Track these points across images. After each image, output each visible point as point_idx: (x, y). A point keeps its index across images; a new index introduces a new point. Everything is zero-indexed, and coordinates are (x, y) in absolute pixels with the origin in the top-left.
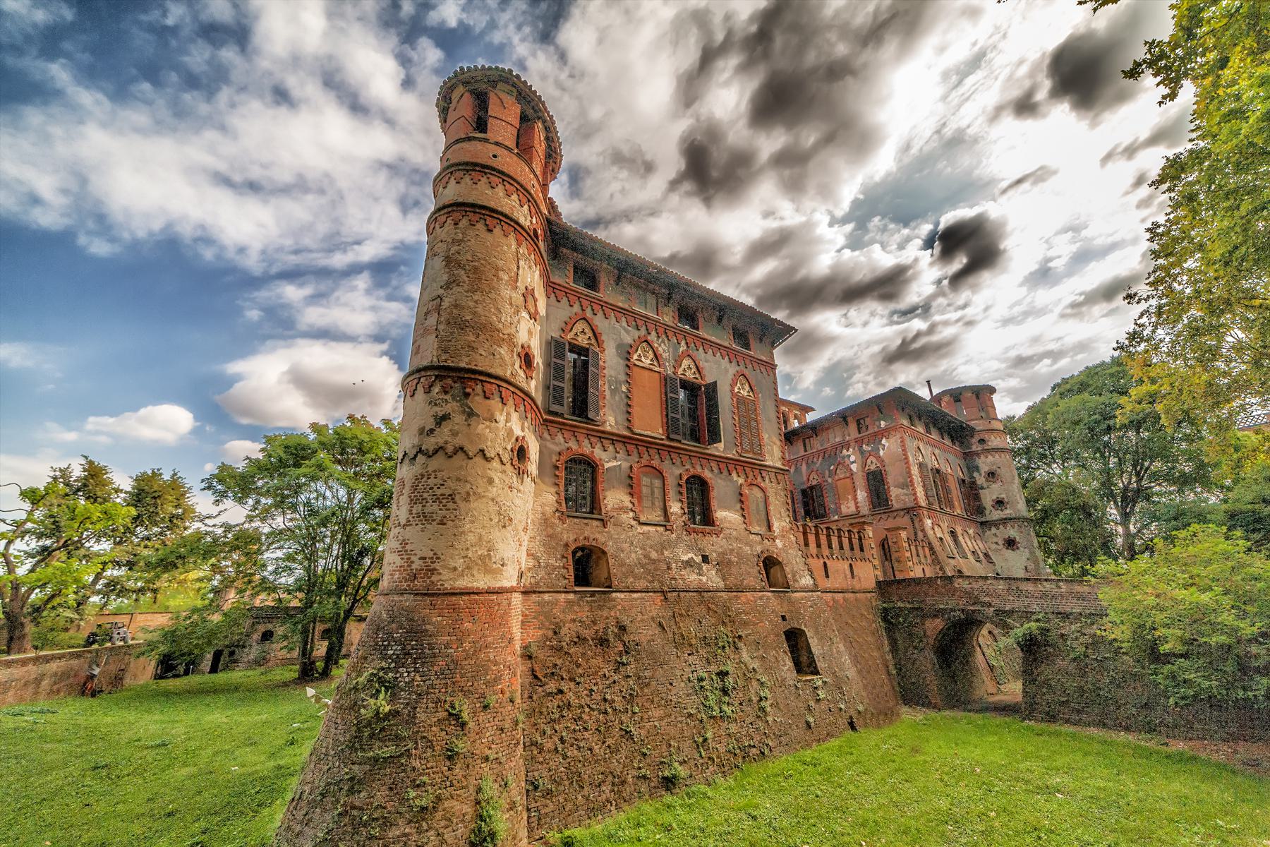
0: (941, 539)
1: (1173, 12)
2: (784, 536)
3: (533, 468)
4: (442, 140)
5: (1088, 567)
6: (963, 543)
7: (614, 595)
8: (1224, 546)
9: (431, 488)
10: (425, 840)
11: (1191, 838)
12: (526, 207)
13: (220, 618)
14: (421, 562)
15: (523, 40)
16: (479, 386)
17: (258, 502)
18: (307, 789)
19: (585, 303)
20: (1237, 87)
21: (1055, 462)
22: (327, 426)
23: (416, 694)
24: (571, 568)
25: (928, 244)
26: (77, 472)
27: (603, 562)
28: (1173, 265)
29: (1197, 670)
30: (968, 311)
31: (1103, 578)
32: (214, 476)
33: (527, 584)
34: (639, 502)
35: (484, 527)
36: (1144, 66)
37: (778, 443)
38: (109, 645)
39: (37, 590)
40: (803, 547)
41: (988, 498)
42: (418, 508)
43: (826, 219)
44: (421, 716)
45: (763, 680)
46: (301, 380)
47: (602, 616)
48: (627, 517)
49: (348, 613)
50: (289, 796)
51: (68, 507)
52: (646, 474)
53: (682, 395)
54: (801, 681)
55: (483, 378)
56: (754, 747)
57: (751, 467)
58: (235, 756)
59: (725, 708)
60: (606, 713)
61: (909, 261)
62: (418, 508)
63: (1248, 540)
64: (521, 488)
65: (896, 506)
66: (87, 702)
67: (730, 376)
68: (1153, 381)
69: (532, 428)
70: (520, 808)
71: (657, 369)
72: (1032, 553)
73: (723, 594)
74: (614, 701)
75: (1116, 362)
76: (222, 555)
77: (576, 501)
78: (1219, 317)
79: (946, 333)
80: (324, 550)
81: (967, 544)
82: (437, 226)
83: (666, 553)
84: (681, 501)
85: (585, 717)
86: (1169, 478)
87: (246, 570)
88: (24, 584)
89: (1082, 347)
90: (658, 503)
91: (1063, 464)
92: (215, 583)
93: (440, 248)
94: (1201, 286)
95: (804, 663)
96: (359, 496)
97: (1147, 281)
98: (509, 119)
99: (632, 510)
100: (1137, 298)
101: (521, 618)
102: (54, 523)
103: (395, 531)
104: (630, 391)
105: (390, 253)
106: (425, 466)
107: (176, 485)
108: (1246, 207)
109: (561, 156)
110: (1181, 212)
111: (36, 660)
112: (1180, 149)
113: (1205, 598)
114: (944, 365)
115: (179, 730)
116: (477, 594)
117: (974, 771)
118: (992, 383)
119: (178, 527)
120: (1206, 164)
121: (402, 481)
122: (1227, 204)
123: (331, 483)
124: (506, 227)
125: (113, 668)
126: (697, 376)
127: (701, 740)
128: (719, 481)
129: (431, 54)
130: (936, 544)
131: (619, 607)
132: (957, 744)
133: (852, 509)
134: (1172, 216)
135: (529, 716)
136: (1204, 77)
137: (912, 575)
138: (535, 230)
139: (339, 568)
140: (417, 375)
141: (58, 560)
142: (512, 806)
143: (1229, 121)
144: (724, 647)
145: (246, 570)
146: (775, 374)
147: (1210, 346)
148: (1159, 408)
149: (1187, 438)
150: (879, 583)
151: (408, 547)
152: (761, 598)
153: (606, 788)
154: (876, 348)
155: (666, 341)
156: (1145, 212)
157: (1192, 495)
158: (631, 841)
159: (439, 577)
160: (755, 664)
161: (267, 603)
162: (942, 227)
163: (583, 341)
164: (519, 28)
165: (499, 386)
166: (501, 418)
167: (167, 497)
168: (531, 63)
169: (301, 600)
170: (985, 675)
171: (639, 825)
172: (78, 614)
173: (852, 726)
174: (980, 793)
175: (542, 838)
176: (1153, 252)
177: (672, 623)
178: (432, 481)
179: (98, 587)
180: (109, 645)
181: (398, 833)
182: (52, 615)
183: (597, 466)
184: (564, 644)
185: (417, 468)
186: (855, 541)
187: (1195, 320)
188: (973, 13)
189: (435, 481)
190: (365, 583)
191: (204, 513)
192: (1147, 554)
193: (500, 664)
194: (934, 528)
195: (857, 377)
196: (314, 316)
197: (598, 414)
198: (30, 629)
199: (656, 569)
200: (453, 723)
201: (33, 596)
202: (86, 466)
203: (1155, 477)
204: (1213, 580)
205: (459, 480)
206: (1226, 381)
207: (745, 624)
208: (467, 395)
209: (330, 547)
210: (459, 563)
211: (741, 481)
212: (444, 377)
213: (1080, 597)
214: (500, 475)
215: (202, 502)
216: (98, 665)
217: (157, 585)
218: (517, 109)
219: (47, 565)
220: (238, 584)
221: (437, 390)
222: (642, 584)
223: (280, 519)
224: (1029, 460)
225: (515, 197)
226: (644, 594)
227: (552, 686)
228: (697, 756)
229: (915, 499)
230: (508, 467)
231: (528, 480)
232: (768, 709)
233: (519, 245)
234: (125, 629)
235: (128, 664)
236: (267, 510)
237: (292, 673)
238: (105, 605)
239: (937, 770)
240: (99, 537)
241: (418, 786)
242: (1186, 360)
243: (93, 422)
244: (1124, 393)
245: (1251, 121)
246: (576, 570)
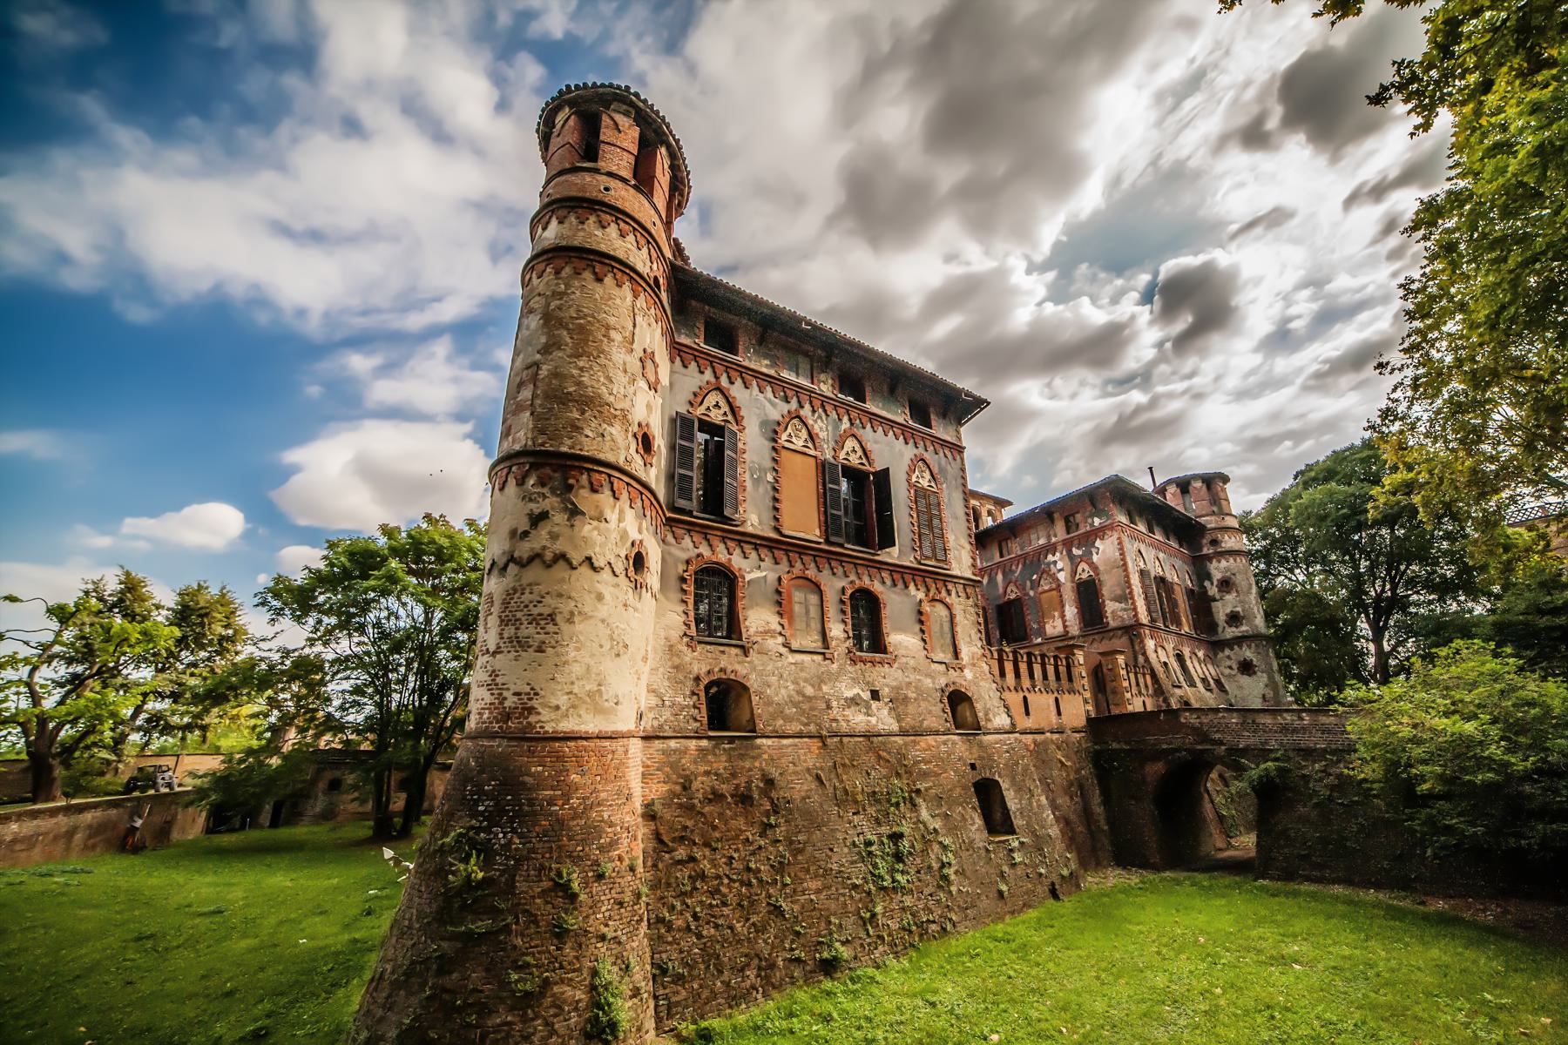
0: (1165, 664)
1: (1428, 26)
2: (974, 665)
3: (653, 578)
4: (542, 172)
5: (1335, 693)
6: (1192, 671)
7: (759, 741)
8: (1492, 665)
9: (527, 606)
10: (531, 1030)
11: (1454, 1016)
12: (645, 250)
13: (279, 762)
14: (515, 699)
15: (644, 51)
16: (585, 477)
17: (320, 622)
18: (389, 967)
19: (720, 369)
20: (1503, 115)
21: (1298, 567)
22: (398, 528)
23: (514, 859)
24: (704, 708)
25: (1147, 298)
26: (112, 585)
27: (745, 700)
28: (1430, 328)
29: (1460, 815)
30: (1196, 381)
31: (1351, 706)
32: (269, 590)
33: (649, 728)
34: (790, 623)
35: (592, 655)
36: (1392, 91)
37: (968, 547)
38: (152, 792)
39: (68, 726)
40: (998, 678)
41: (1221, 611)
42: (509, 631)
43: (1023, 265)
44: (521, 886)
45: (946, 842)
46: (368, 471)
47: (743, 767)
48: (775, 644)
49: (430, 759)
50: (367, 975)
51: (102, 626)
52: (798, 587)
53: (844, 485)
54: (993, 842)
55: (590, 466)
56: (934, 922)
57: (933, 577)
58: (301, 927)
59: (899, 877)
60: (749, 884)
61: (1126, 317)
62: (509, 631)
63: (1521, 658)
64: (639, 606)
65: (1112, 624)
66: (126, 861)
67: (906, 461)
68: (1410, 468)
69: (652, 529)
70: (645, 995)
71: (812, 452)
72: (1271, 678)
73: (897, 738)
74: (759, 870)
75: (1367, 444)
76: (280, 686)
77: (709, 623)
78: (1484, 391)
79: (1172, 407)
80: (398, 682)
81: (1197, 669)
82: (534, 275)
83: (825, 688)
84: (844, 622)
85: (724, 890)
86: (1430, 586)
87: (308, 704)
88: (52, 718)
89: (1330, 425)
90: (815, 625)
91: (1307, 569)
92: (273, 719)
93: (537, 303)
94: (1463, 353)
95: (997, 820)
96: (438, 615)
97: (1401, 348)
98: (625, 145)
99: (780, 634)
100: (1389, 368)
101: (641, 769)
102: (86, 646)
103: (482, 660)
104: (777, 481)
105: (476, 311)
106: (518, 577)
107: (223, 600)
108: (1515, 258)
109: (690, 187)
110: (1438, 265)
111: (67, 810)
112: (1433, 192)
113: (1470, 727)
114: (1169, 448)
115: (237, 894)
116: (586, 739)
117: (1197, 941)
118: (1225, 471)
119: (228, 651)
120: (1467, 207)
121: (490, 596)
122: (1493, 255)
123: (404, 598)
124: (619, 275)
125: (157, 819)
126: (864, 461)
127: (868, 915)
128: (893, 596)
129: (531, 72)
130: (1160, 670)
131: (766, 756)
132: (1178, 911)
133: (1059, 629)
134: (1427, 270)
135: (653, 888)
136: (1463, 103)
137: (1130, 708)
138: (656, 278)
139: (417, 704)
140: (507, 464)
141: (91, 690)
142: (636, 993)
143: (1494, 156)
144: (897, 804)
145: (308, 704)
146: (962, 459)
147: (1474, 426)
148: (1416, 499)
149: (1449, 536)
150: (1089, 720)
151: (499, 680)
152: (945, 743)
153: (751, 973)
154: (1087, 426)
155: (824, 417)
156: (1397, 265)
157: (1455, 604)
158: (782, 1033)
159: (538, 718)
160: (937, 824)
161: (333, 745)
162: (1161, 277)
163: (716, 417)
164: (640, 37)
165: (610, 476)
166: (612, 516)
167: (215, 614)
168: (652, 78)
169: (372, 743)
170: (1214, 829)
171: (791, 1015)
172: (116, 755)
173: (1054, 894)
174: (1203, 966)
175: (672, 1030)
176: (1408, 313)
177: (833, 776)
178: (527, 597)
179: (139, 722)
180: (152, 792)
181: (498, 1021)
182: (86, 755)
183: (736, 577)
184: (696, 801)
185: (508, 581)
186: (1062, 669)
187: (1457, 394)
188: (1189, 25)
189: (531, 597)
190: (448, 723)
191: (258, 636)
192: (1402, 677)
193: (616, 825)
194: (1159, 651)
195: (1065, 462)
196: (385, 391)
197: (736, 511)
198: (59, 772)
199: (812, 709)
200: (560, 894)
201: (63, 733)
202: (123, 578)
203: (1412, 583)
204: (1479, 706)
205: (560, 595)
206: (1493, 467)
207: (925, 775)
208: (570, 488)
209: (405, 677)
210: (563, 701)
211: (921, 595)
212: (542, 465)
213: (1326, 730)
214: (612, 589)
215: (254, 621)
216: (140, 817)
217: (207, 720)
218: (635, 132)
219: (78, 696)
220: (299, 722)
221: (532, 482)
222: (794, 727)
223: (345, 643)
224: (1268, 564)
225: (631, 238)
226: (797, 740)
227: (681, 853)
228: (863, 934)
229: (1136, 615)
230: (622, 579)
231: (647, 596)
232: (953, 877)
233: (636, 296)
234: (170, 773)
235: (174, 817)
236: (329, 632)
237: (364, 830)
238: (147, 744)
239: (1154, 941)
240: (139, 661)
241: (521, 967)
242: (1446, 442)
243: (131, 525)
244: (1377, 481)
245: (1520, 156)
246: (709, 709)
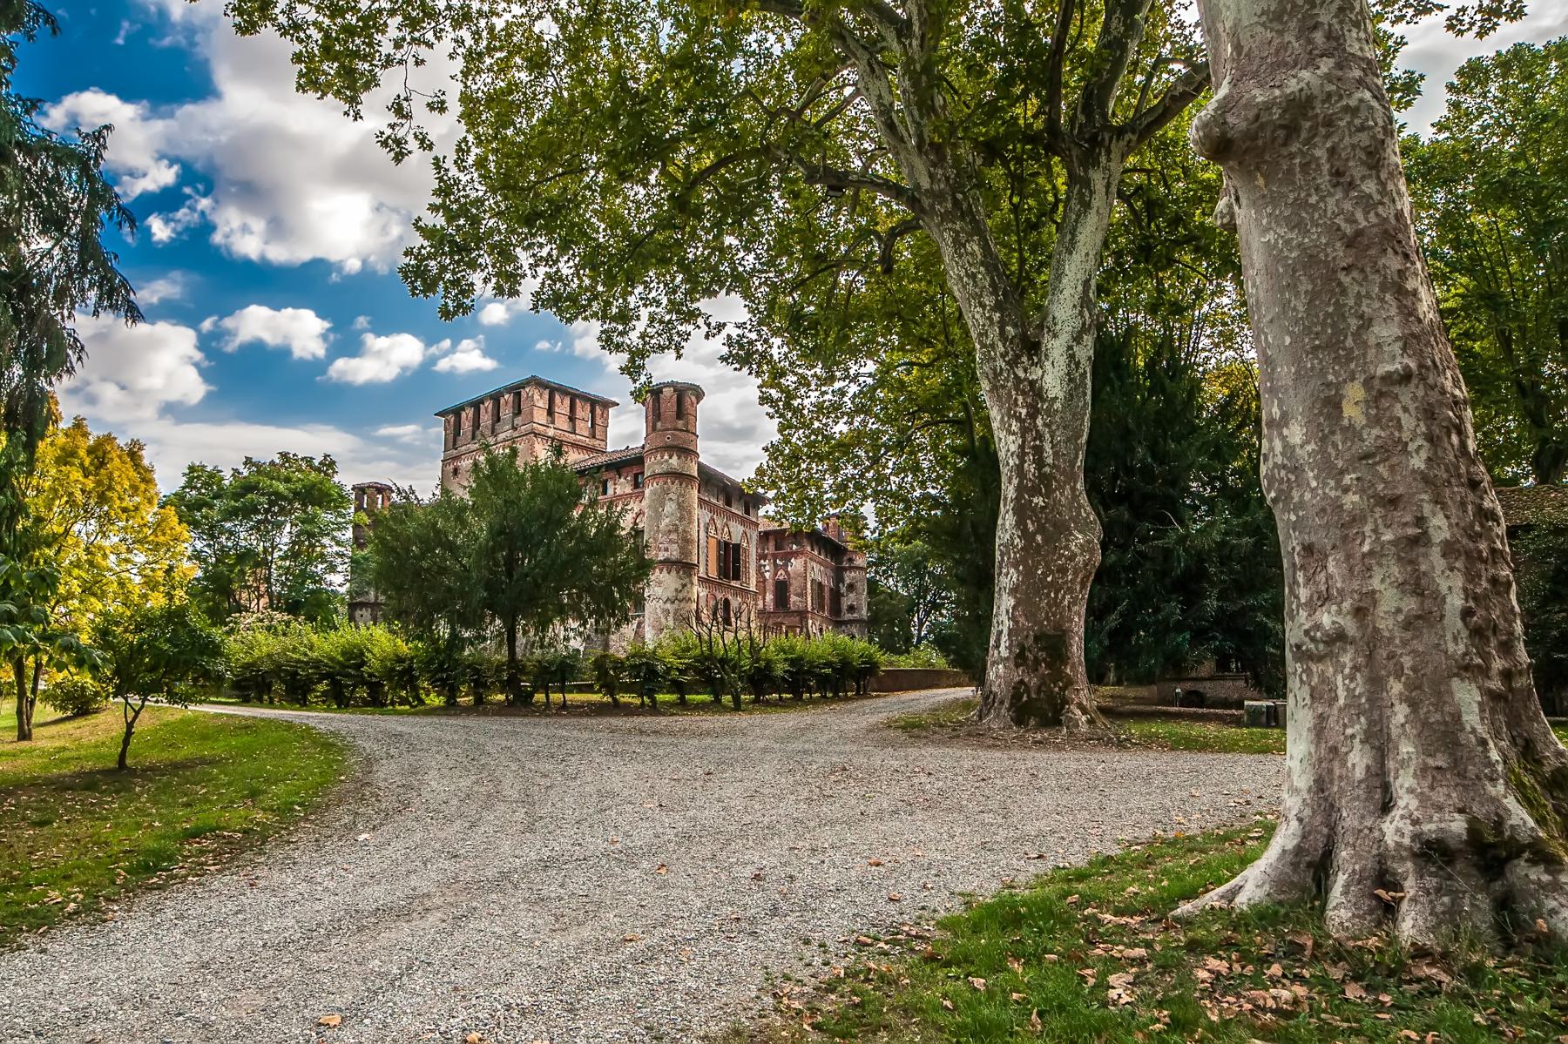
41: (846, 602)
